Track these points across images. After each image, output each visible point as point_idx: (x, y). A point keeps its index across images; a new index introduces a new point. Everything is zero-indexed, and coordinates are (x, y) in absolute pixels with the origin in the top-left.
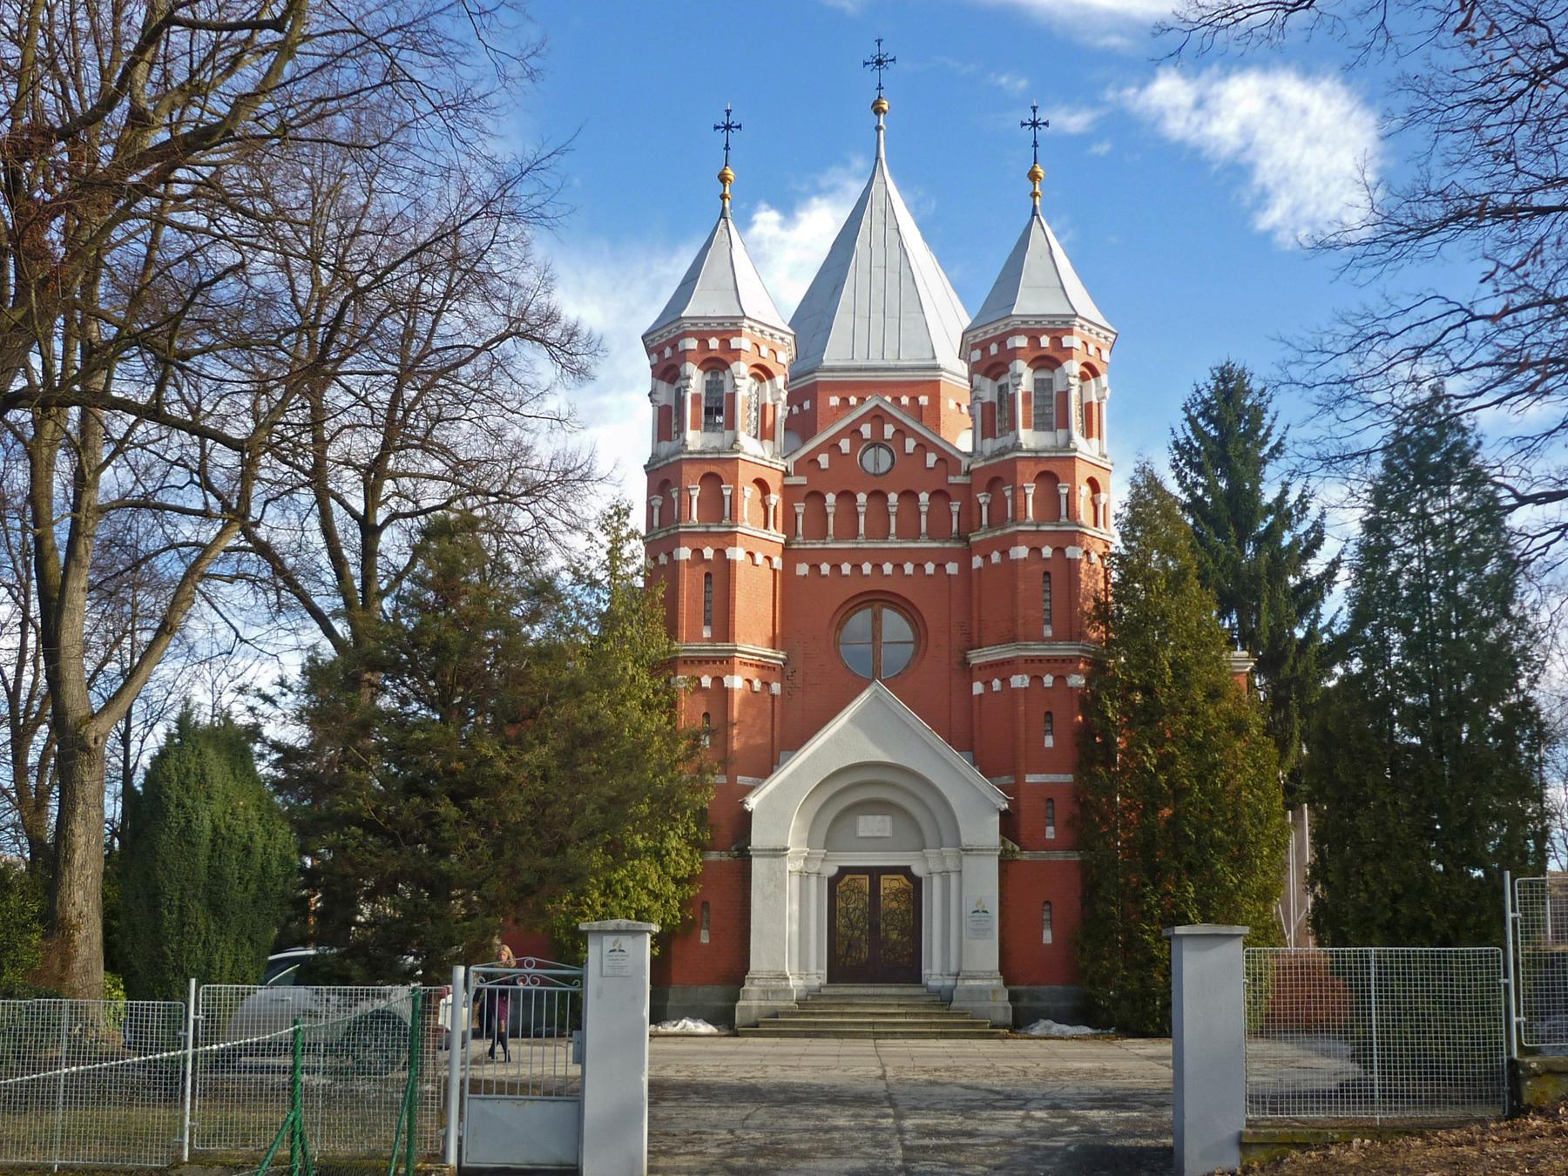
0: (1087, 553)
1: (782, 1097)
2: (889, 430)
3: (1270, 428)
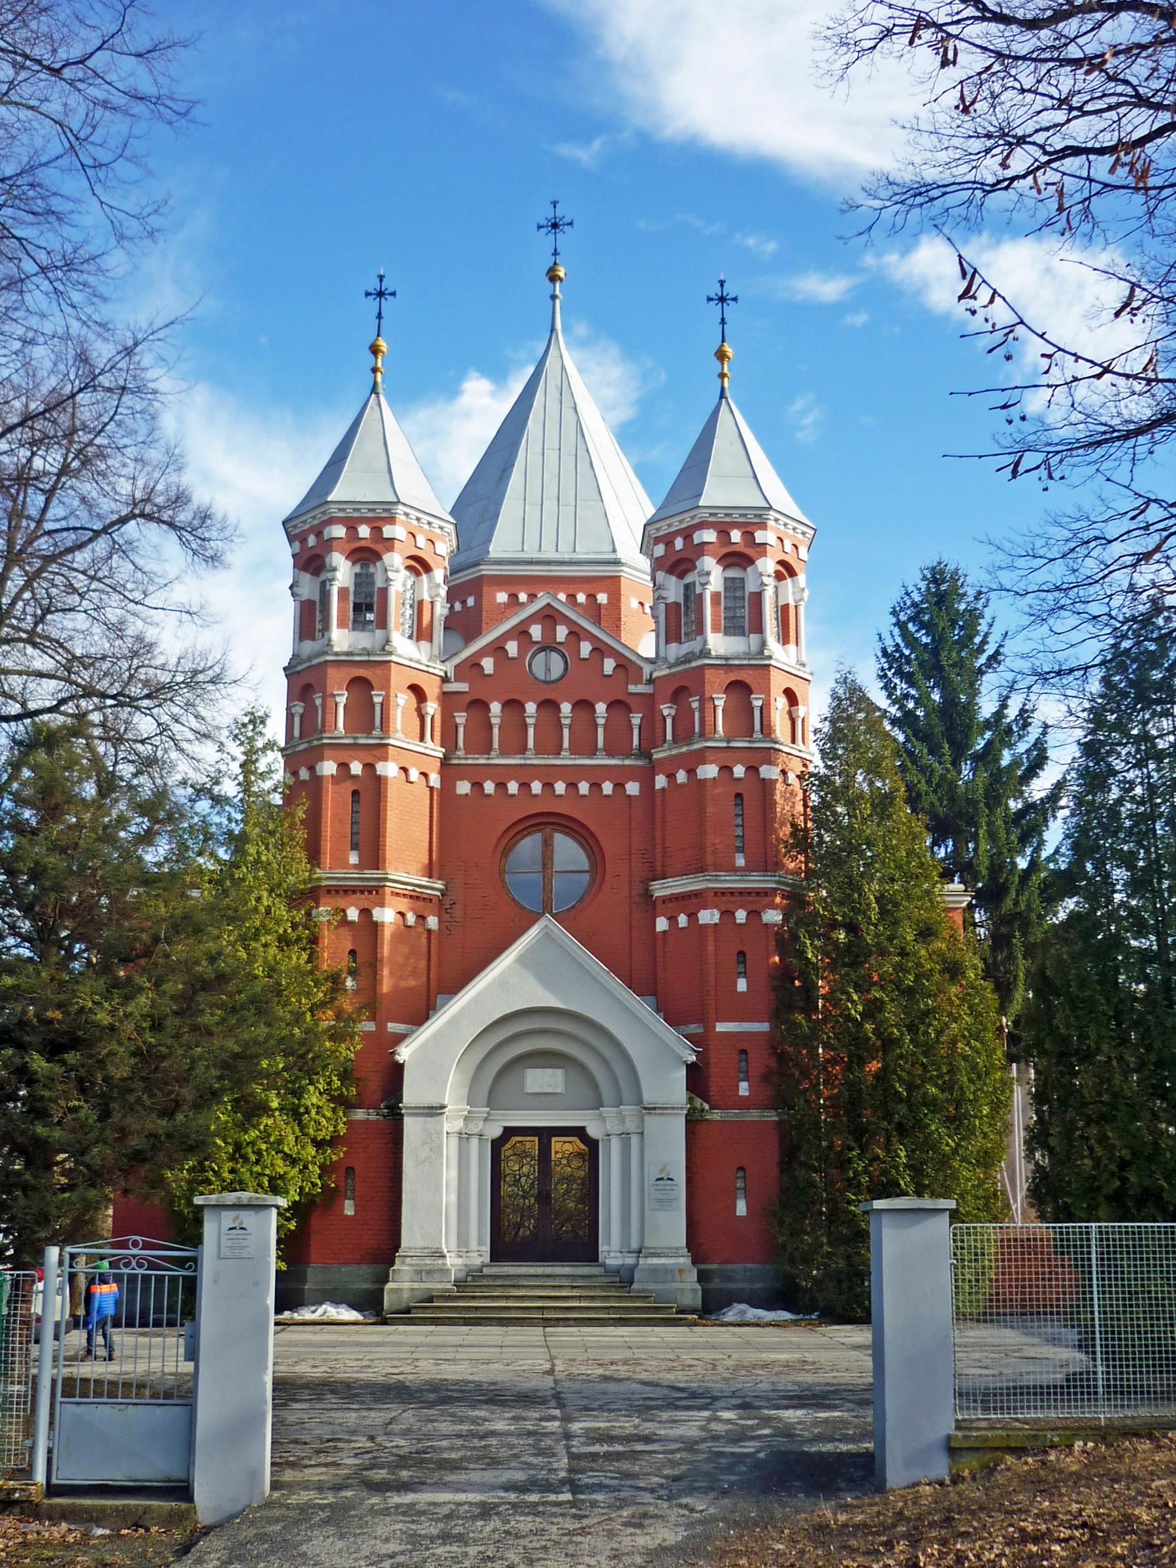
0: (784, 772)
1: (432, 1396)
2: (562, 632)
3: (986, 635)
